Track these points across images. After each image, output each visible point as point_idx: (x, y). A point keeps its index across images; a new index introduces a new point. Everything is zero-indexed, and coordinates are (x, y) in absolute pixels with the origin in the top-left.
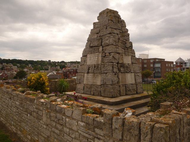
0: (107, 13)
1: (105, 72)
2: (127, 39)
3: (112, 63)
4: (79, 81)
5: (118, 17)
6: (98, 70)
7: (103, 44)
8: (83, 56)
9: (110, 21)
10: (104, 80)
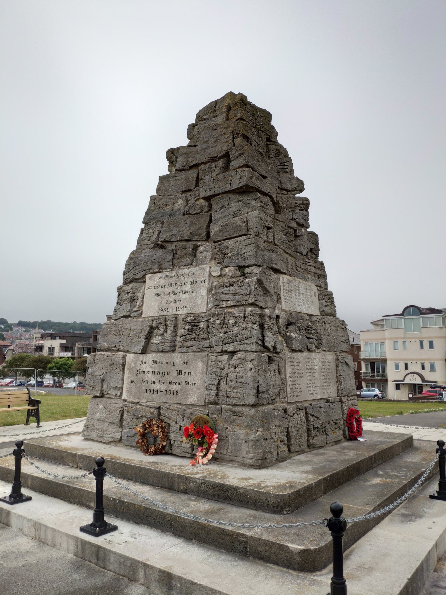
0: (229, 108)
1: (230, 347)
2: (302, 221)
3: (258, 311)
4: (98, 388)
5: (270, 134)
6: (195, 339)
7: (214, 229)
8: (126, 282)
9: (239, 141)
10: (223, 383)
